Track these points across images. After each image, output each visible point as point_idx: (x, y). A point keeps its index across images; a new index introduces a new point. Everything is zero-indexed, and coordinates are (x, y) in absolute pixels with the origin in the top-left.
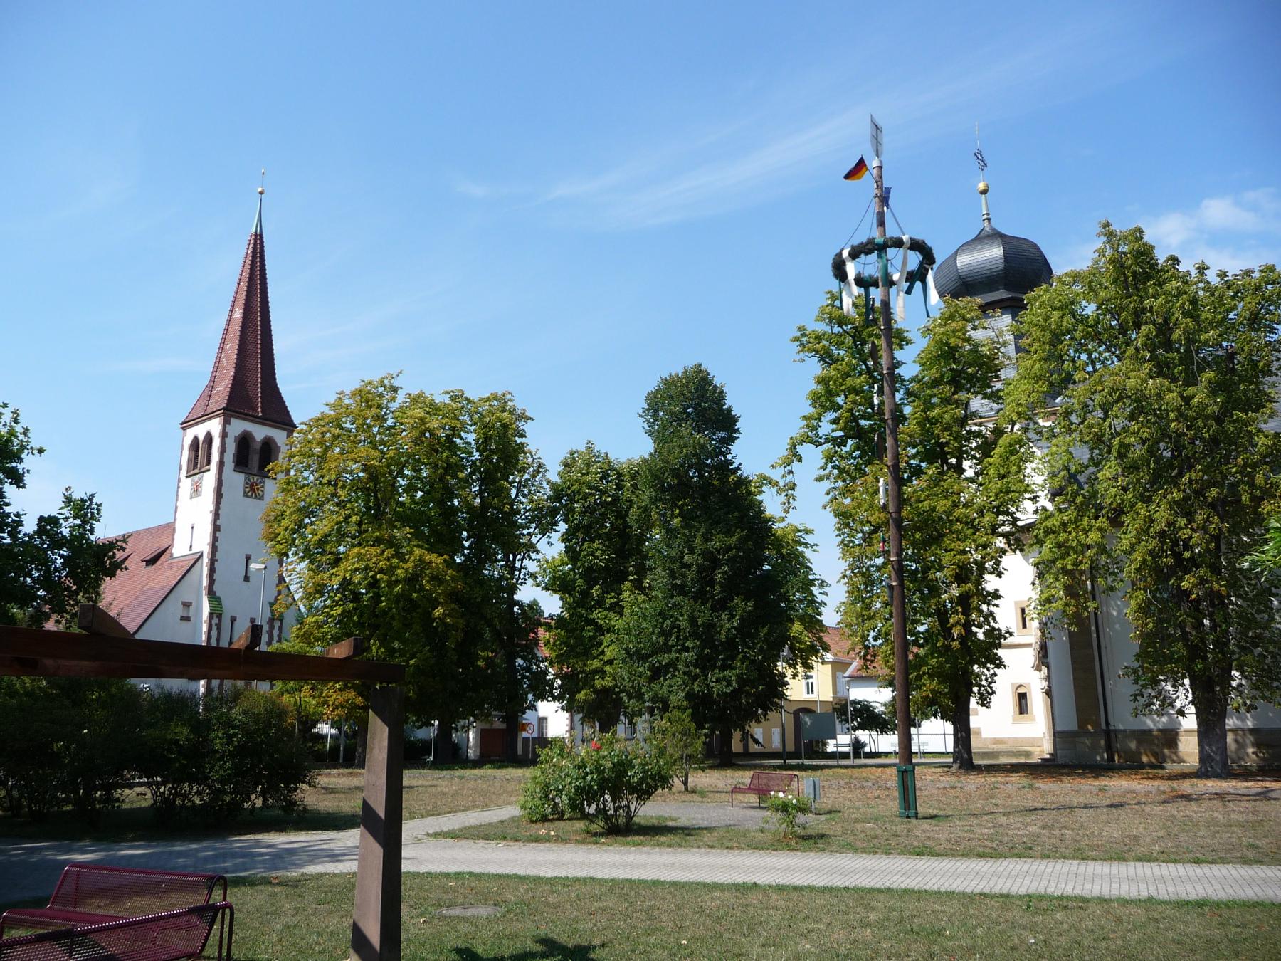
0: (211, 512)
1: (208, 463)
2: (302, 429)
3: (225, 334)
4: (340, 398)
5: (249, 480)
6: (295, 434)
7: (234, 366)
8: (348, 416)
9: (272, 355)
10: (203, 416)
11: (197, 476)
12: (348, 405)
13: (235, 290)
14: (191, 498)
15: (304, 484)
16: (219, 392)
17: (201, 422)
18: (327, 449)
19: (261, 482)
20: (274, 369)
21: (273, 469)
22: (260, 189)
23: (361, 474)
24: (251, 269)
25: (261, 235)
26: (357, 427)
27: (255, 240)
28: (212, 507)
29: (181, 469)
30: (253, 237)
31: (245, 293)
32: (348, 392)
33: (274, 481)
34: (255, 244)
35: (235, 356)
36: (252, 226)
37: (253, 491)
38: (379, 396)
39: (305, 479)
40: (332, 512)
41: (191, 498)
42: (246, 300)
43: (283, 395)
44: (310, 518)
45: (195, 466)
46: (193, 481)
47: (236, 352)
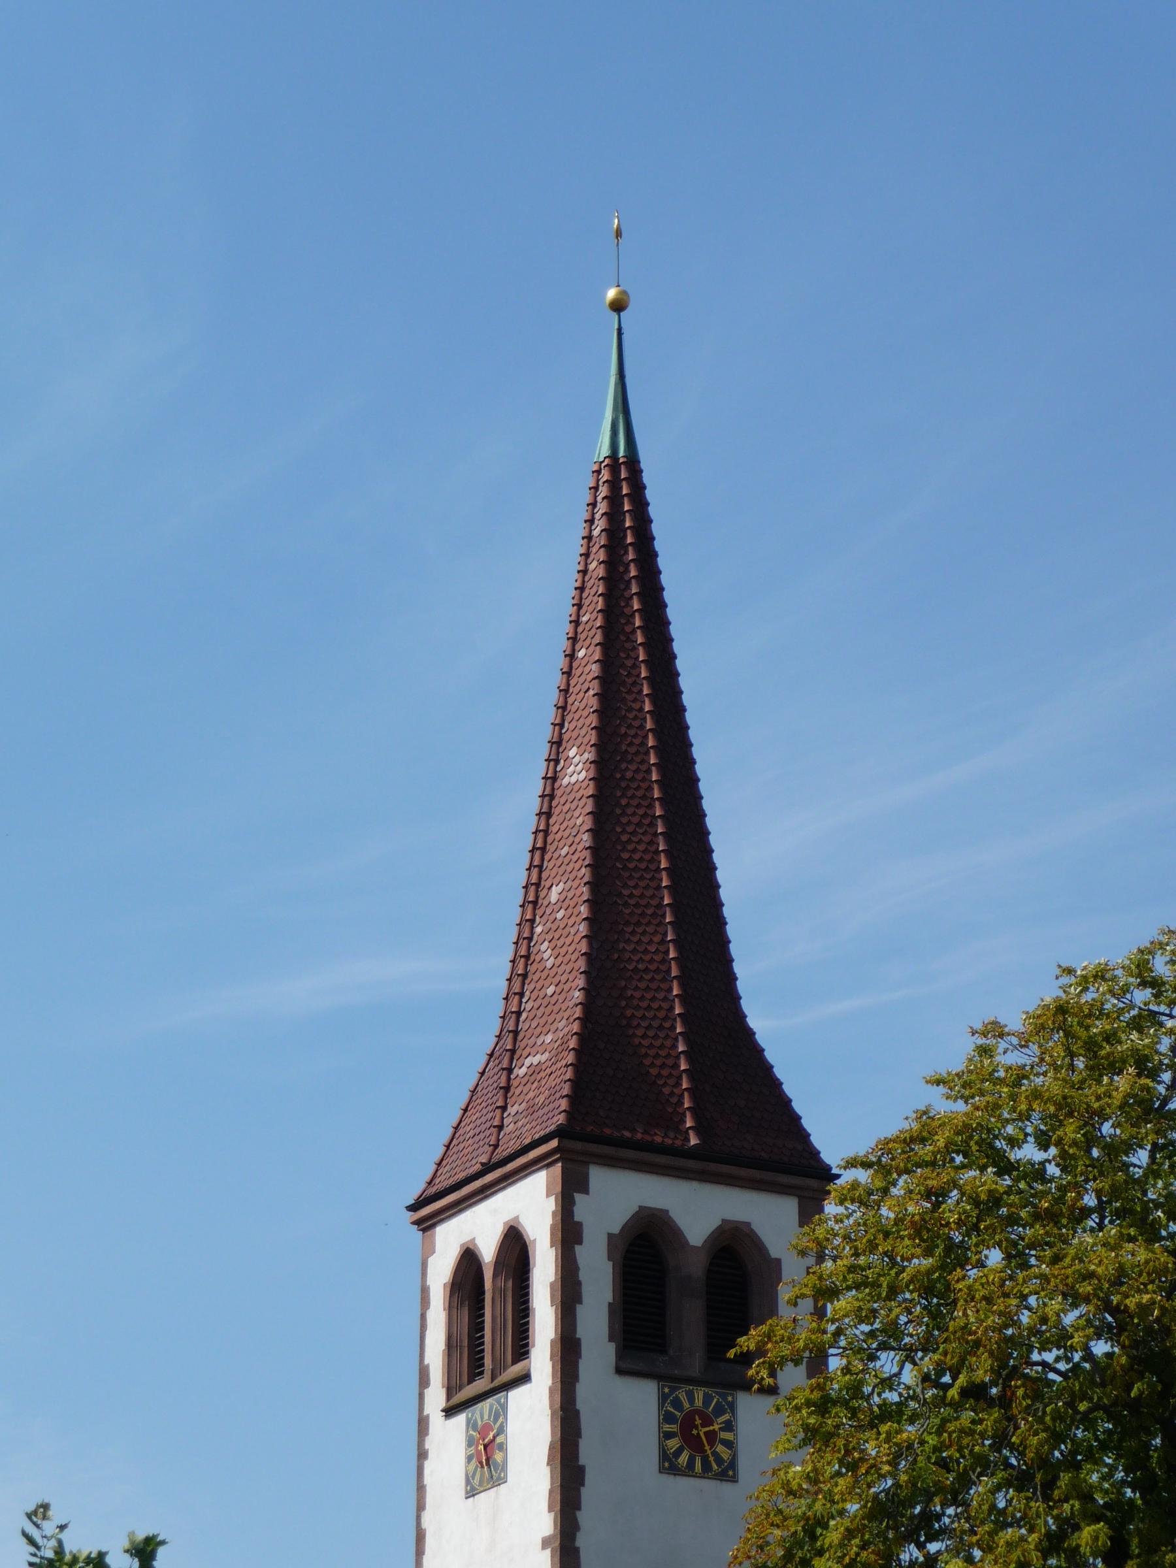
0: (546, 1543)
1: (522, 1348)
2: (855, 1185)
3: (540, 850)
4: (984, 1051)
5: (677, 1404)
6: (831, 1208)
7: (582, 964)
8: (1025, 1116)
9: (716, 905)
10: (487, 1168)
11: (486, 1405)
12: (1020, 1076)
13: (558, 679)
14: (471, 1493)
15: (884, 1405)
16: (535, 1070)
17: (484, 1193)
18: (955, 1257)
19: (719, 1411)
20: (727, 961)
21: (761, 1352)
22: (611, 293)
23: (1100, 1348)
24: (607, 596)
25: (633, 463)
26: (1063, 1155)
27: (614, 484)
28: (545, 1523)
29: (424, 1380)
30: (605, 475)
31: (595, 687)
32: (1015, 1022)
33: (769, 1402)
34: (614, 499)
35: (583, 929)
36: (598, 432)
37: (693, 1443)
38: (1137, 1024)
39: (888, 1383)
40: (1002, 1520)
41: (471, 1493)
42: (601, 713)
43: (769, 1055)
44: (921, 1546)
45: (475, 1369)
46: (471, 1424)
47: (584, 910)
